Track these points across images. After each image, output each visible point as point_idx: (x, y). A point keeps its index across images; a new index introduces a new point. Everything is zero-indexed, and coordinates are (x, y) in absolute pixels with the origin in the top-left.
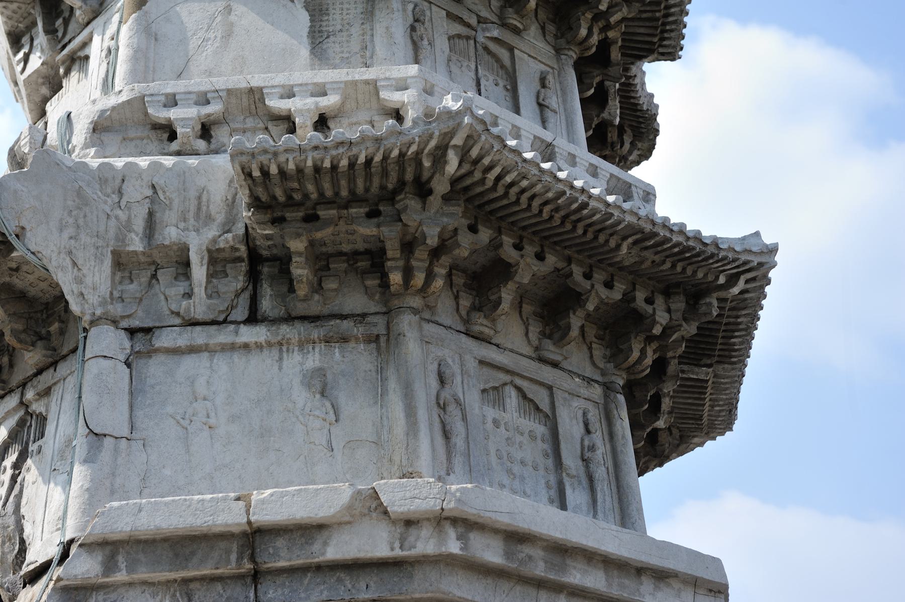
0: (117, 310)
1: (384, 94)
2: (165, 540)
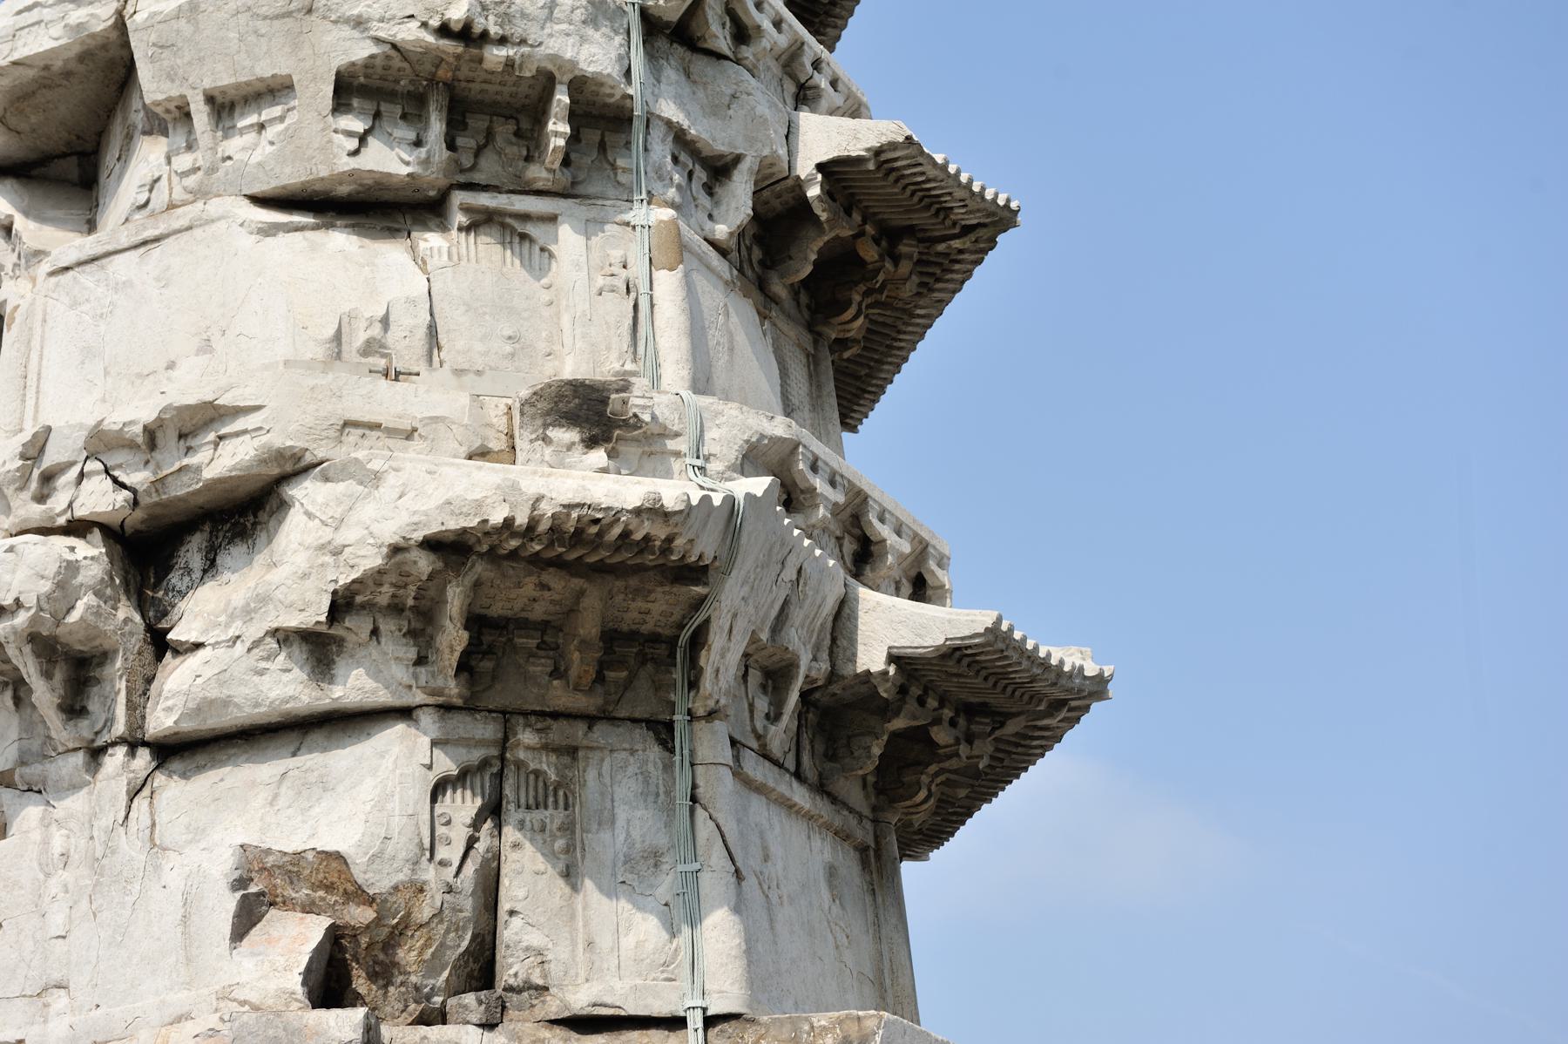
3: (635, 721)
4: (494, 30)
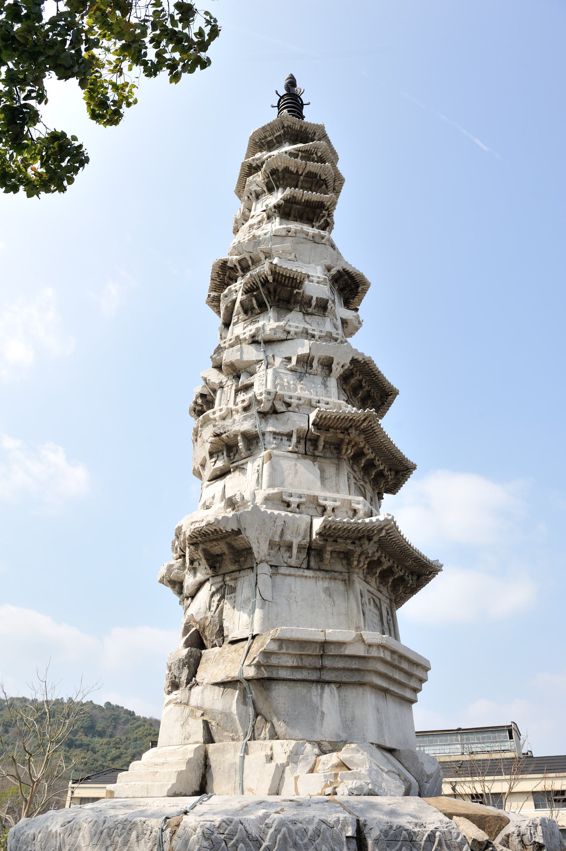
0: (268, 558)
1: (353, 505)
2: (297, 641)
3: (248, 568)
4: (222, 431)
